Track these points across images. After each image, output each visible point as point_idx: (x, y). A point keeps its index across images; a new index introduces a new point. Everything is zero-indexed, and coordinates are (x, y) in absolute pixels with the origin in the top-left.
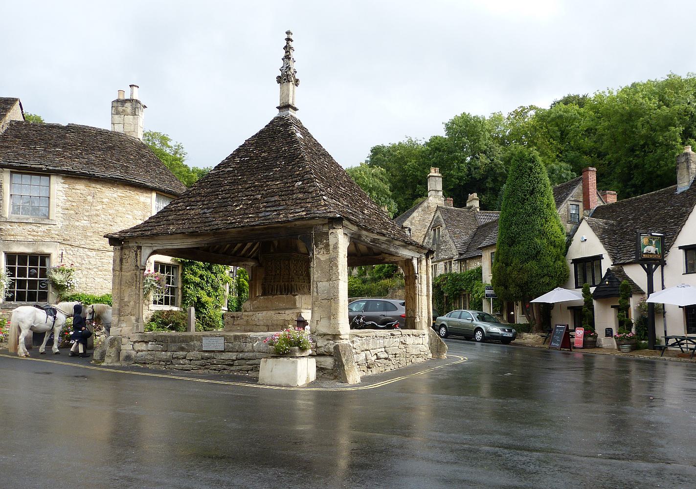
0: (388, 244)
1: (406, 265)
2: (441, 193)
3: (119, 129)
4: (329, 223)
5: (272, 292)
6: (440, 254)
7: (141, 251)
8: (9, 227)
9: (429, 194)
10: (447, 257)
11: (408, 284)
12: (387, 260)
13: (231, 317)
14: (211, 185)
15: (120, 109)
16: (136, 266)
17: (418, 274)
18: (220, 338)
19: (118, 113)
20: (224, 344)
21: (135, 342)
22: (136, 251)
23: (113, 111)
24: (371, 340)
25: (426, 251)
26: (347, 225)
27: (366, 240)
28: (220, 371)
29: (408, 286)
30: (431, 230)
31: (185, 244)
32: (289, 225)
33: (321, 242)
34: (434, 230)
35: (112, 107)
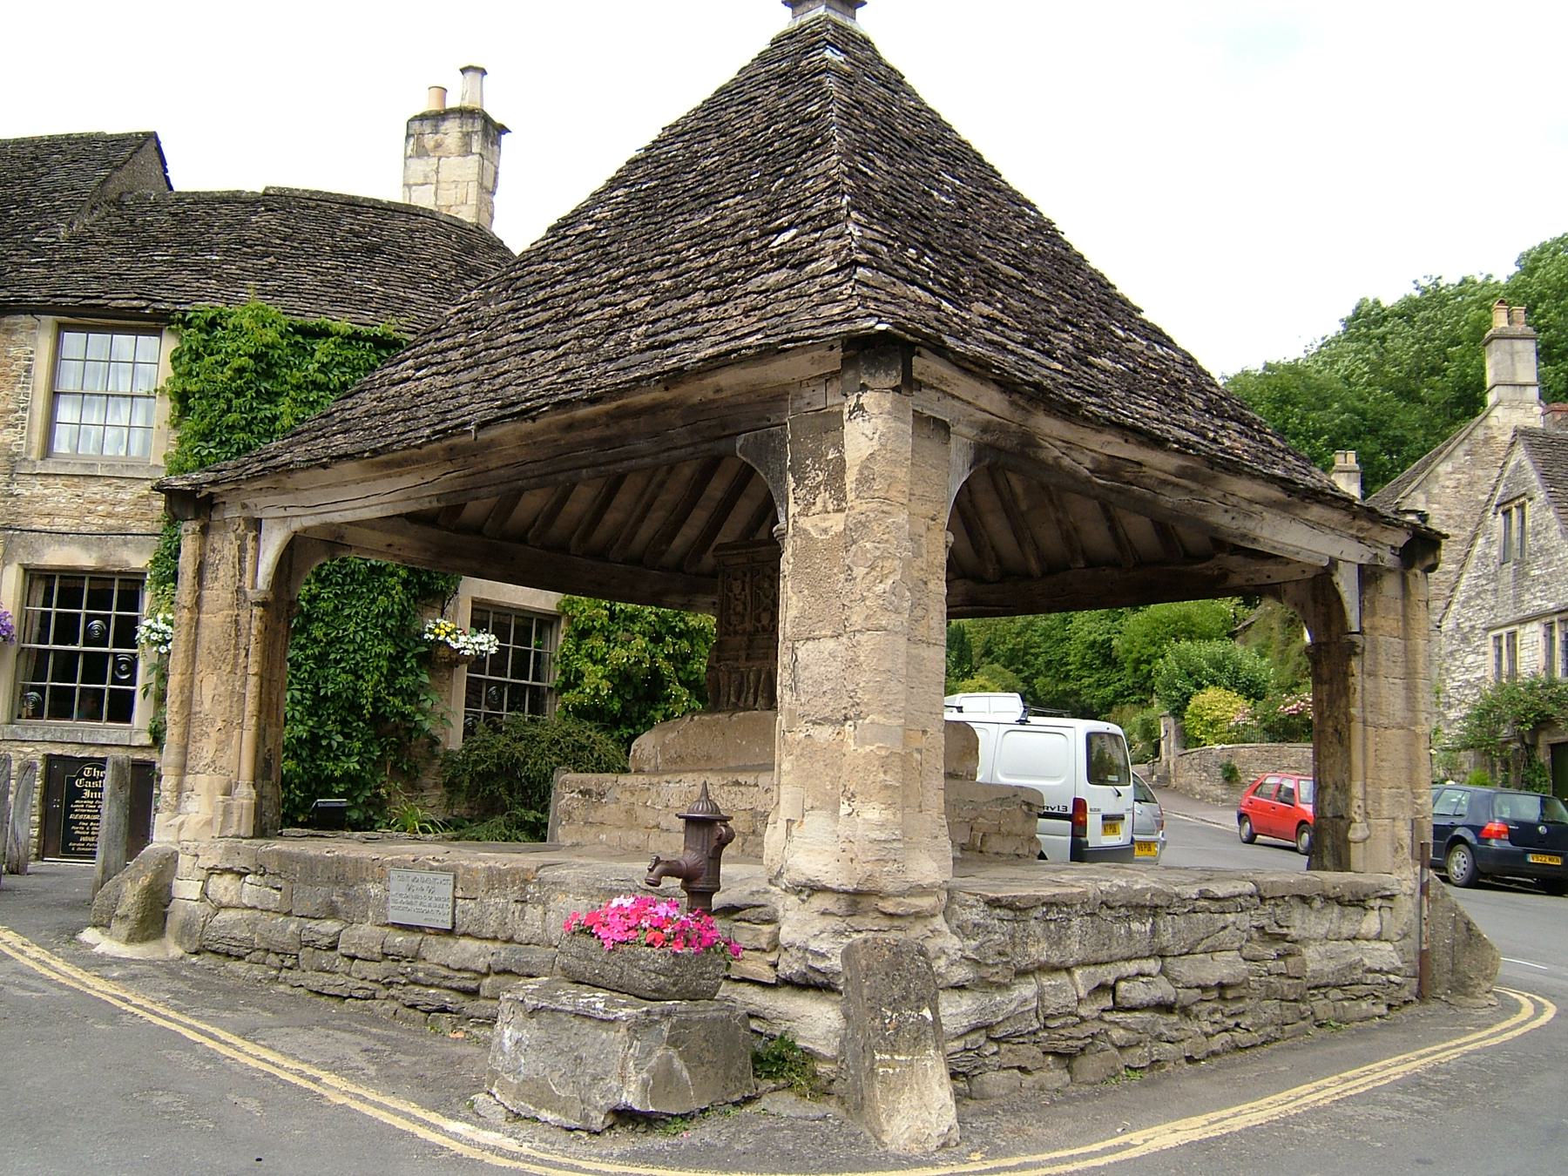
0: (1191, 492)
1: (1315, 601)
2: (1533, 393)
3: (423, 199)
4: (847, 363)
5: (738, 699)
6: (1527, 597)
7: (257, 539)
8: (39, 490)
9: (1491, 398)
10: (1551, 605)
11: (1325, 677)
12: (1236, 580)
13: (580, 792)
14: (515, 291)
15: (429, 140)
16: (239, 590)
17: (1361, 632)
18: (442, 877)
19: (421, 152)
20: (455, 902)
21: (212, 871)
22: (242, 539)
23: (409, 148)
24: (1076, 922)
25: (1401, 538)
26: (941, 380)
27: (1066, 461)
28: (429, 1012)
29: (1326, 687)
30: (1495, 514)
31: (374, 500)
32: (697, 392)
33: (818, 456)
34: (1504, 513)
35: (408, 136)
